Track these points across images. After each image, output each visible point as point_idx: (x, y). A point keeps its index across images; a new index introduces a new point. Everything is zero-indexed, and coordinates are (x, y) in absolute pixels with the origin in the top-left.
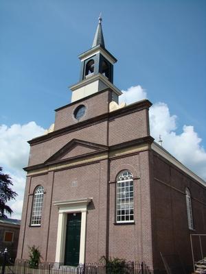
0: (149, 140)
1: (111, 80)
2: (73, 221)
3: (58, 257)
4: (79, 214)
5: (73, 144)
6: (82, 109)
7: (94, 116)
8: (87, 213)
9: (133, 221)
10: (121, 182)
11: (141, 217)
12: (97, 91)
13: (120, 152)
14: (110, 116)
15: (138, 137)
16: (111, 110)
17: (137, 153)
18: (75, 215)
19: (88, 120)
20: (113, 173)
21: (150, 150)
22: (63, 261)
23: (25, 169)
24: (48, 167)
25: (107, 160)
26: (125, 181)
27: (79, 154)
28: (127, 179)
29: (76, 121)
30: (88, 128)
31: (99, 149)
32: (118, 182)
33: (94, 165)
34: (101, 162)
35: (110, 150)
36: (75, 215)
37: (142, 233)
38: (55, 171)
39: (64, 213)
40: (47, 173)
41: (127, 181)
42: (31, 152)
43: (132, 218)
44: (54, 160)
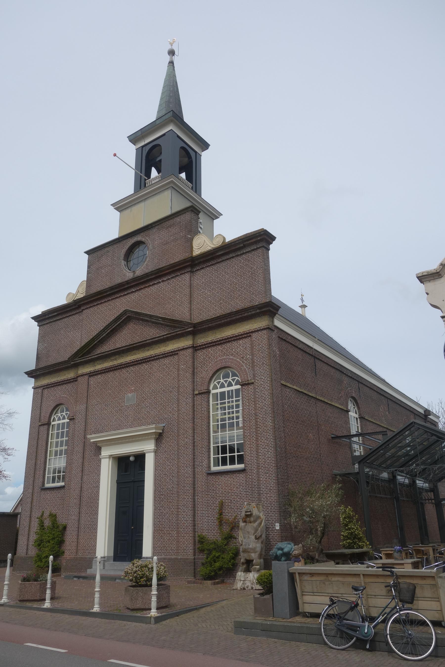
0: (271, 308)
1: (197, 188)
2: (130, 469)
3: (103, 544)
4: (140, 458)
5: (126, 319)
6: (142, 247)
7: (163, 264)
8: (156, 452)
9: (242, 466)
10: (219, 390)
11: (258, 457)
12: (115, 235)
13: (135, 354)
14: (194, 263)
15: (247, 304)
16: (196, 252)
17: (247, 335)
18: (132, 459)
19: (152, 273)
20: (204, 373)
21: (271, 329)
22: (112, 554)
23: (30, 374)
24: (76, 366)
25: (190, 350)
26: (226, 389)
27: (137, 339)
28: (230, 385)
29: (129, 275)
30: (154, 289)
31: (177, 328)
32: (53, 423)
33: (166, 361)
34: (254, 335)
35: (197, 329)
36: (132, 459)
37: (259, 488)
38: (91, 375)
39: (110, 456)
40: (75, 380)
41: (230, 388)
42: (42, 338)
43: (241, 459)
44: (86, 354)
